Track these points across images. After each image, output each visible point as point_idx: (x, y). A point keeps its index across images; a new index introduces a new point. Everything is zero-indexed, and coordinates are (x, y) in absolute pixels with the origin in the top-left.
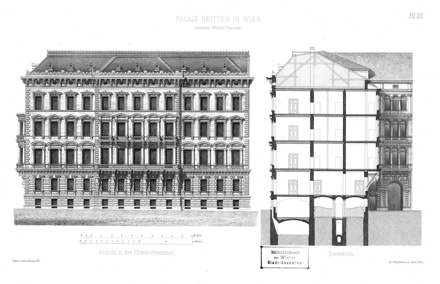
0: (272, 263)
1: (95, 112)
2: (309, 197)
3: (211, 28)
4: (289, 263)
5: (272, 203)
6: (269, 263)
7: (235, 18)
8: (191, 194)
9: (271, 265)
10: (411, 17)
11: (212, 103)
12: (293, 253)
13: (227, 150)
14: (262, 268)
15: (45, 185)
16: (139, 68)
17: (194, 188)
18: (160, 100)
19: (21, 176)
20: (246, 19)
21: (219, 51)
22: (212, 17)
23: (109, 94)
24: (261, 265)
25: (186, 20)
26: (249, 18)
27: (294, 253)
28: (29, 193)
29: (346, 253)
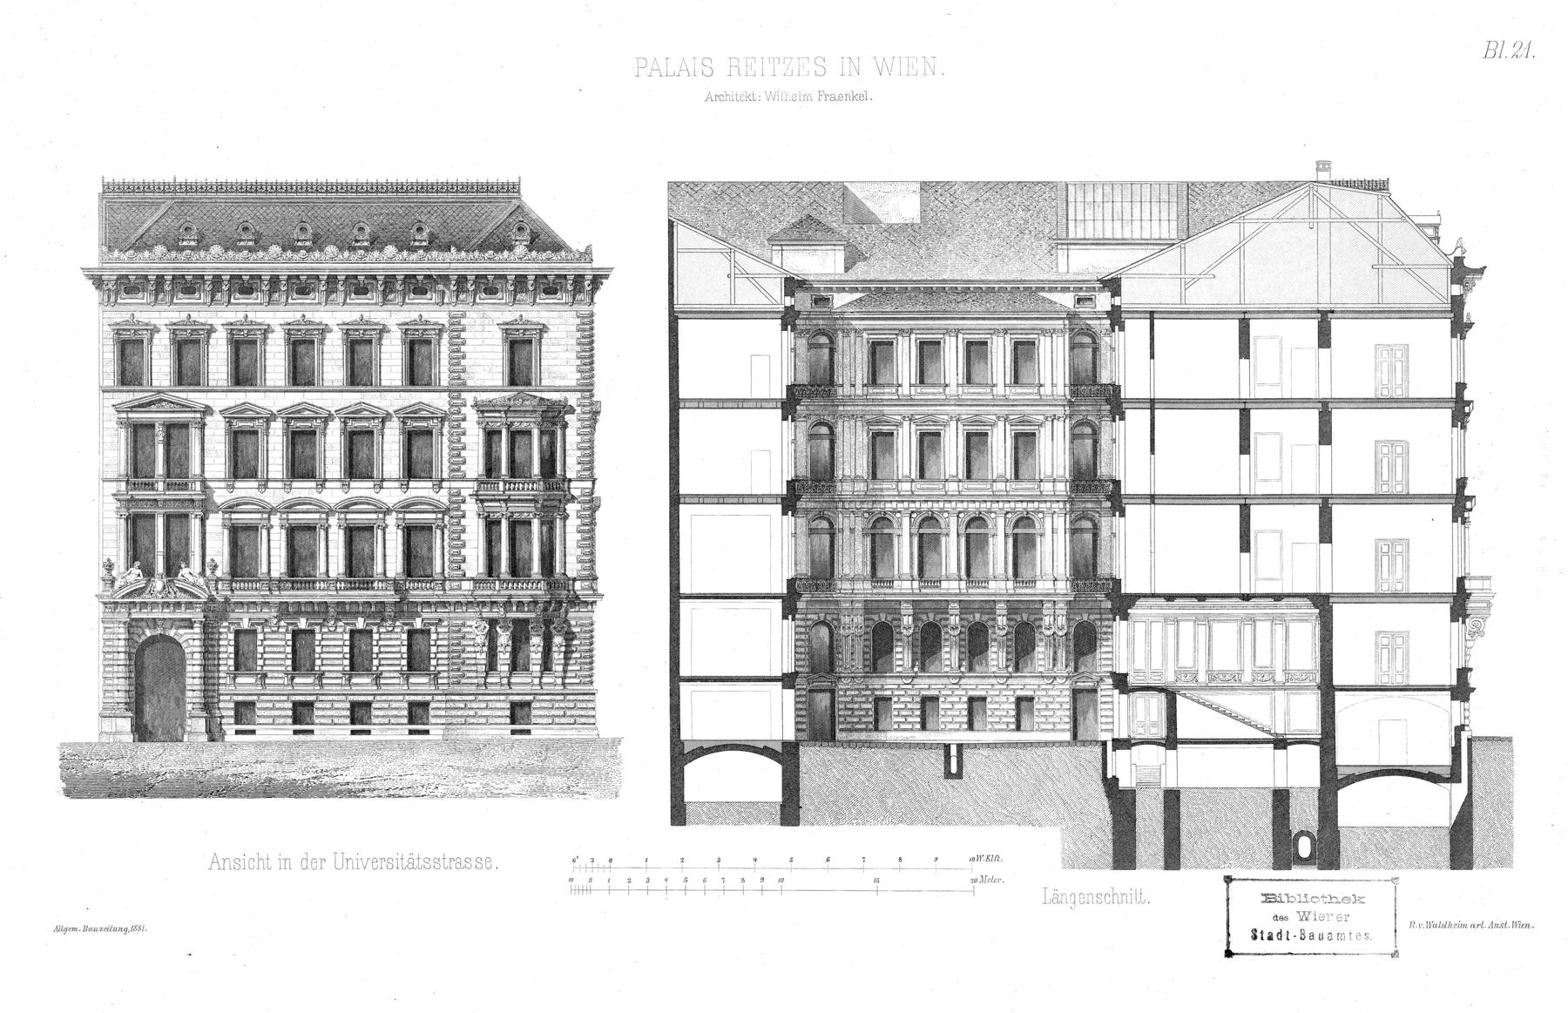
0: (1265, 936)
1: (450, 391)
2: (1449, 693)
3: (764, 98)
4: (1325, 936)
5: (1467, 714)
6: (1255, 938)
7: (847, 61)
8: (313, 684)
9: (1262, 945)
10: (1491, 54)
11: (332, 362)
12: (1340, 900)
13: (330, 526)
14: (1229, 954)
15: (271, 652)
16: (425, 235)
17: (267, 662)
18: (268, 348)
21: (372, 180)
22: (766, 61)
23: (374, 330)
24: (1228, 943)
25: (670, 73)
26: (897, 61)
27: (1346, 899)
28: (463, 681)
29: (1123, 895)
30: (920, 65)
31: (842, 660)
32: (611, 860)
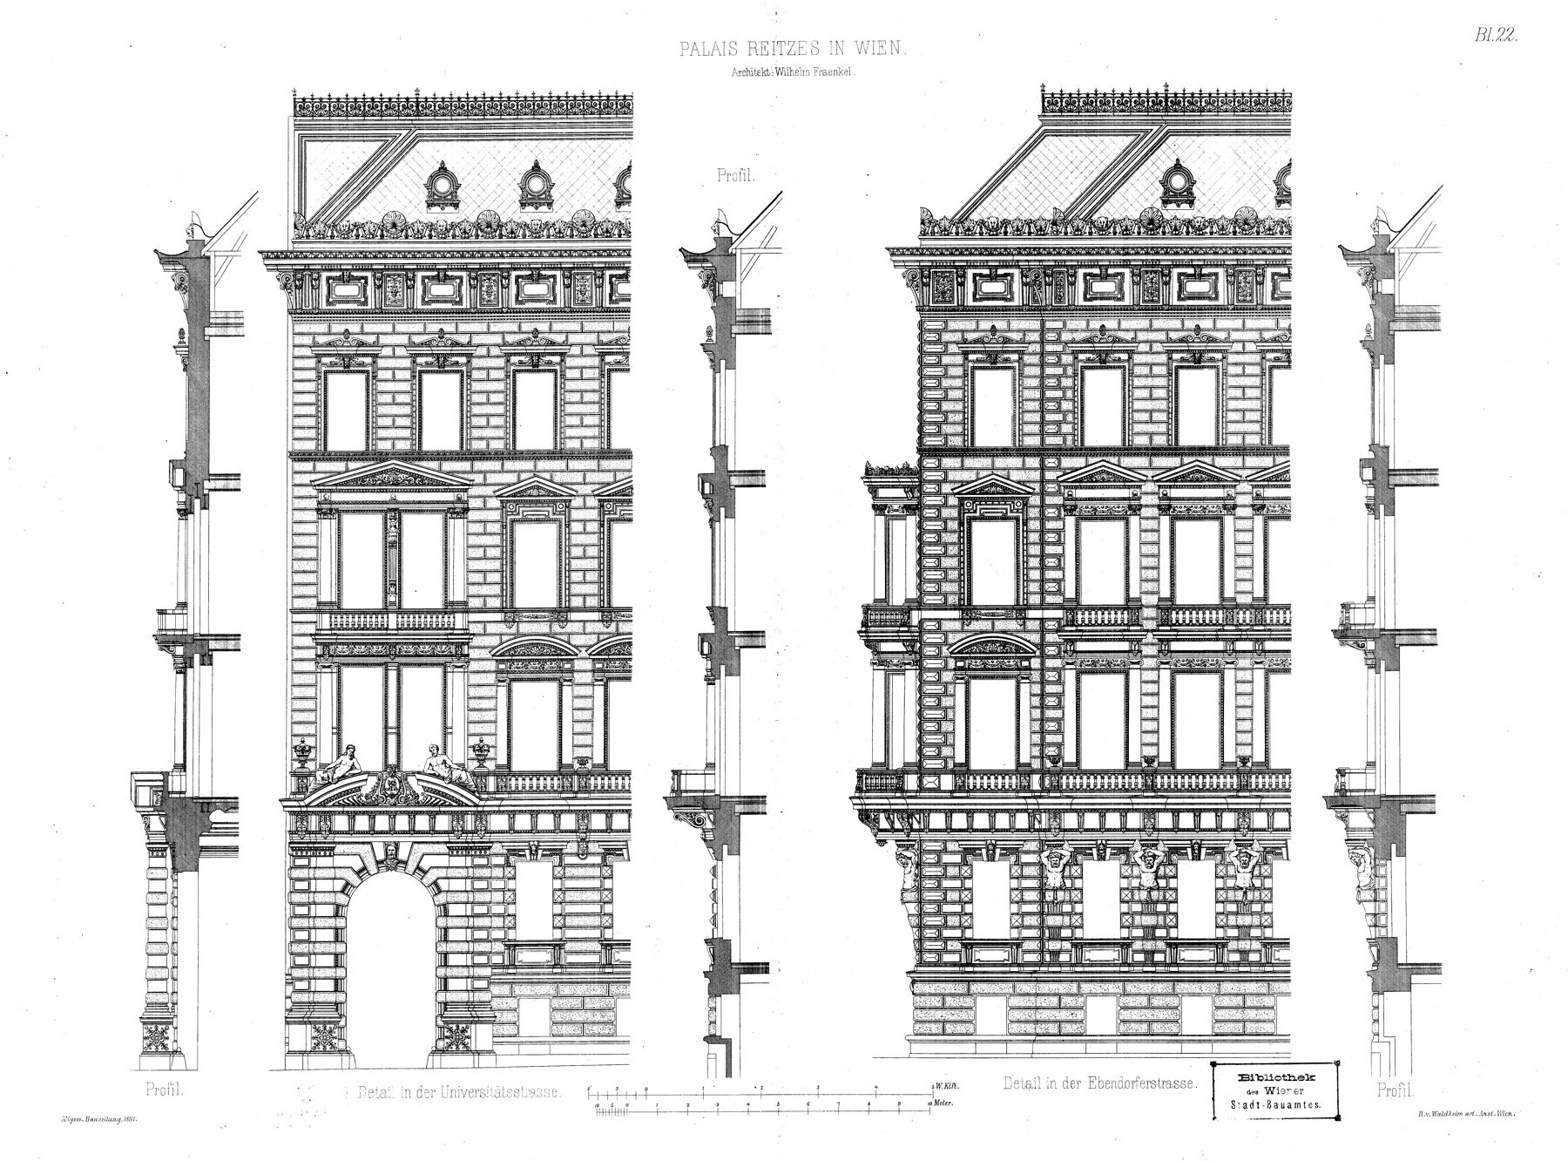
4: (1286, 1106)
19: (891, 846)
20: (862, 48)
27: (1301, 1078)
30: (888, 47)
31: (1385, 877)
32: (646, 1089)
